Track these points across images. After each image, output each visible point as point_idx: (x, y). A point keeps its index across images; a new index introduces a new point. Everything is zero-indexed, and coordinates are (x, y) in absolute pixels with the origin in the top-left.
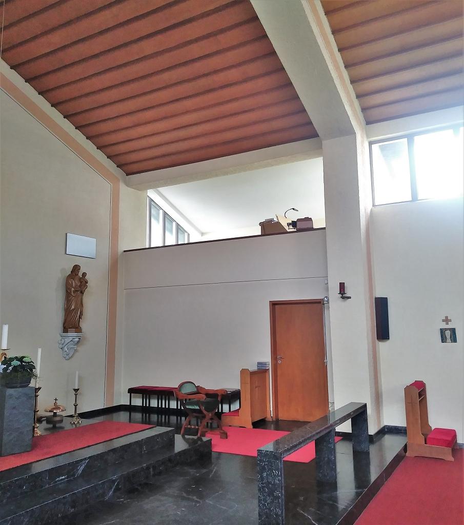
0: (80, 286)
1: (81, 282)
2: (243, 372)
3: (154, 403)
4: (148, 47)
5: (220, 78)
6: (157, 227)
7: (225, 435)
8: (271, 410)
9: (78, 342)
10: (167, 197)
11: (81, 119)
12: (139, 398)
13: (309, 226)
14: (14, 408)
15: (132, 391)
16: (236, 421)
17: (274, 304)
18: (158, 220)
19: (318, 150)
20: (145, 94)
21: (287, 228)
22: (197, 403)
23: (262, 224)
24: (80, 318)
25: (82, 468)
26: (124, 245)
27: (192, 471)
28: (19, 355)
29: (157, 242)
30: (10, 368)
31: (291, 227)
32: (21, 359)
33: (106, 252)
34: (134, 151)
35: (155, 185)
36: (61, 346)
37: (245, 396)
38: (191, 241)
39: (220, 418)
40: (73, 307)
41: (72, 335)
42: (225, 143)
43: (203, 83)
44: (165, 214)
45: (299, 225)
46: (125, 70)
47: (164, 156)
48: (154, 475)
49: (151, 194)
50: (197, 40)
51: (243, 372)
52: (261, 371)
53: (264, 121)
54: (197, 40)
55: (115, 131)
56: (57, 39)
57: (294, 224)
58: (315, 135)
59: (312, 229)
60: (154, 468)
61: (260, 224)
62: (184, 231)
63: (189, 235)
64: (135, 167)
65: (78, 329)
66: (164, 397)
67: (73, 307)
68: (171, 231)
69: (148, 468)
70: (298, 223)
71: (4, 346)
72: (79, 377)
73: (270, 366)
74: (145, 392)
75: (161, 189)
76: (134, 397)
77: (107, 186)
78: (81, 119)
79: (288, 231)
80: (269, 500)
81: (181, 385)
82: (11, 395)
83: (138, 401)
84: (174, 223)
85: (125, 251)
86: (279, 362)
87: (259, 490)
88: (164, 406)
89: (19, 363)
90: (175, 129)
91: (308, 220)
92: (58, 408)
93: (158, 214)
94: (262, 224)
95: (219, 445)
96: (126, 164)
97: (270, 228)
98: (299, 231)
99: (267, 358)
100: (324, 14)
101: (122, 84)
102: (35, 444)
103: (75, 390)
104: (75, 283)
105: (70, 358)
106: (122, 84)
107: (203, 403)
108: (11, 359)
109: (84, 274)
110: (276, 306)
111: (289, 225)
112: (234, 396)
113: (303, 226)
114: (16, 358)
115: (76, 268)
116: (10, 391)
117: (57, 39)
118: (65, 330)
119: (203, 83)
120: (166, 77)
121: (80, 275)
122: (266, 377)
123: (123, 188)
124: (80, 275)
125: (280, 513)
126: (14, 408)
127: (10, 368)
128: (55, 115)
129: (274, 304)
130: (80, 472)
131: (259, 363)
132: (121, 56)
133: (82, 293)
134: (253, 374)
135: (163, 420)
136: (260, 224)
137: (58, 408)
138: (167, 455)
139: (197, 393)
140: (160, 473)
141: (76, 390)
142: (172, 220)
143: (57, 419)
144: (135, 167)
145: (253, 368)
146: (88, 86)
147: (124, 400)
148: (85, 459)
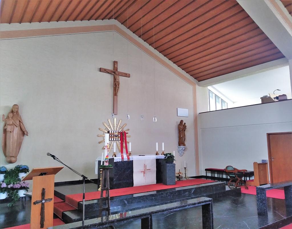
0: (184, 128)
1: (184, 127)
2: (255, 163)
3: (216, 176)
4: (206, 33)
5: (238, 39)
6: (212, 101)
7: (247, 188)
8: (270, 180)
9: (185, 150)
10: (216, 88)
11: (180, 63)
12: (210, 173)
13: (285, 98)
14: (169, 170)
15: (206, 170)
16: (252, 184)
17: (269, 135)
18: (213, 98)
19: (287, 62)
20: (205, 50)
21: (274, 99)
22: (234, 174)
23: (262, 98)
24: (184, 140)
25: (193, 191)
26: (199, 111)
27: (233, 197)
28: (169, 153)
29: (213, 109)
30: (167, 157)
31: (276, 99)
32: (170, 154)
33: (192, 114)
34: (200, 68)
35: (211, 84)
36: (178, 151)
37: (256, 174)
38: (228, 108)
39: (245, 183)
40: (182, 136)
41: (182, 147)
42: (241, 64)
43: (230, 42)
44: (216, 95)
45: (280, 98)
46: (197, 43)
47: (214, 72)
48: (218, 197)
49: (209, 88)
50: (226, 27)
51: (255, 163)
52: (264, 164)
53: (259, 53)
54: (226, 27)
55: (194, 65)
56: (171, 37)
57: (277, 98)
58: (283, 57)
59: (287, 100)
60: (218, 194)
61: (261, 98)
62: (225, 102)
63: (227, 103)
64: (202, 78)
65: (184, 145)
66: (220, 173)
67: (182, 136)
68: (219, 102)
69: (216, 194)
70: (279, 97)
71: (157, 150)
72: (186, 163)
73: (268, 162)
74: (212, 171)
75: (214, 86)
76: (208, 173)
77: (191, 87)
78: (180, 63)
79: (275, 101)
80: (261, 204)
81: (227, 167)
82: (168, 166)
83: (209, 175)
84: (220, 99)
85: (199, 113)
86: (273, 160)
87: (257, 201)
88: (220, 177)
89: (170, 155)
90: (217, 52)
91: (284, 95)
92: (181, 173)
93: (213, 95)
94: (262, 98)
95: (243, 190)
96: (198, 77)
97: (266, 100)
98: (280, 101)
99: (266, 158)
100: (284, 7)
101: (196, 48)
102: (176, 183)
103: (185, 168)
104: (182, 127)
105: (182, 156)
106: (196, 48)
107: (237, 174)
108: (167, 154)
109: (185, 124)
110: (270, 135)
111: (275, 98)
112: (251, 174)
113: (282, 99)
114: (168, 154)
115: (182, 121)
116: (168, 164)
117: (171, 37)
118: (179, 145)
119: (230, 42)
120: (214, 43)
121: (183, 124)
122: (266, 166)
123: (197, 87)
124: (183, 124)
125: (265, 209)
126: (169, 170)
127: (167, 157)
128: (170, 63)
129: (269, 135)
130: (192, 192)
131: (262, 160)
132: (195, 38)
133: (185, 131)
134: (259, 164)
135: (220, 175)
136: (261, 98)
137: (181, 173)
138: (223, 191)
139: (234, 170)
140: (221, 197)
141: (185, 168)
142: (219, 97)
143: (180, 177)
144: (202, 78)
145: (260, 162)
146: (182, 51)
147: (204, 174)
148: (194, 188)
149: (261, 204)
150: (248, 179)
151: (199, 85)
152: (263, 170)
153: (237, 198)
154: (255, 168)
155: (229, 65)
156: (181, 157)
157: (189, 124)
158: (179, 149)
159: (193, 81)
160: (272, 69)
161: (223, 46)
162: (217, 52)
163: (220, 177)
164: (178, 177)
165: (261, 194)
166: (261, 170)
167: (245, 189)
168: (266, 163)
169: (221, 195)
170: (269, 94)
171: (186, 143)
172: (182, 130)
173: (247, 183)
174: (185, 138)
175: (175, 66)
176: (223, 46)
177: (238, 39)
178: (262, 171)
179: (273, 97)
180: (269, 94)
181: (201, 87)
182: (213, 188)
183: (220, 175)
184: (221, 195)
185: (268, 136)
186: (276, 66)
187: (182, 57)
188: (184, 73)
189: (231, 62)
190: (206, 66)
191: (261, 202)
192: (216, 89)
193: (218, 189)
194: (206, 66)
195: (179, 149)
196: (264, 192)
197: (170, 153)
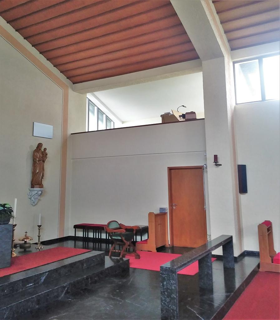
1: (43, 154)
2: (150, 214)
3: (91, 235)
5: (136, 20)
12: (80, 231)
15: (76, 227)
16: (146, 247)
17: (170, 169)
19: (199, 67)
24: (42, 178)
26: (71, 130)
35: (92, 90)
37: (152, 231)
39: (135, 245)
40: (37, 171)
42: (138, 63)
43: (123, 23)
44: (98, 109)
45: (187, 117)
49: (89, 96)
51: (150, 214)
52: (162, 214)
57: (183, 116)
58: (197, 57)
59: (196, 119)
60: (91, 278)
63: (114, 123)
65: (41, 185)
67: (37, 171)
69: (87, 278)
70: (186, 115)
77: (60, 91)
79: (180, 120)
80: (168, 300)
81: (109, 223)
83: (80, 234)
85: (72, 134)
86: (174, 208)
88: (97, 237)
91: (193, 113)
92: (27, 238)
93: (94, 109)
95: (134, 263)
96: (74, 76)
97: (168, 119)
98: (187, 120)
99: (166, 205)
104: (39, 155)
106: (71, 24)
107: (124, 235)
109: (45, 149)
111: (180, 116)
112: (144, 230)
113: (189, 117)
115: (40, 145)
118: (33, 186)
119: (123, 23)
120: (100, 19)
121: (42, 149)
123: (70, 91)
128: (27, 45)
129: (170, 169)
130: (42, 280)
131: (161, 209)
133: (44, 161)
134: (157, 215)
135: (97, 234)
137: (27, 238)
138: (100, 270)
141: (39, 226)
142: (103, 113)
143: (27, 245)
145: (157, 212)
147: (71, 233)
148: (46, 272)
149: (168, 300)
150: (139, 238)
151: (74, 90)
152: (161, 224)
153: (125, 280)
154: (150, 221)
155: (120, 62)
156: (35, 207)
157: (52, 151)
158: (31, 193)
159: (64, 82)
160: (178, 75)
161: (114, 27)
162: (105, 54)
163: (97, 237)
164: (21, 246)
165: (168, 280)
166: (159, 225)
167: (136, 258)
168: (166, 213)
169: (96, 279)
170: (172, 111)
171: (45, 183)
172: (39, 161)
173: (138, 246)
174: (43, 176)
175: (34, 52)
176: (114, 27)
177: (136, 20)
178: (159, 225)
179: (177, 115)
180: (172, 111)
181: (75, 93)
182: (83, 265)
183: (97, 234)
184: (96, 279)
185: (170, 172)
186: (184, 71)
187: (47, 37)
188: (49, 65)
189: (125, 57)
190: (85, 59)
191: (169, 296)
192: (99, 99)
193: (93, 265)
194: (85, 59)
195: (31, 193)
196: (174, 276)
197: (5, 204)
